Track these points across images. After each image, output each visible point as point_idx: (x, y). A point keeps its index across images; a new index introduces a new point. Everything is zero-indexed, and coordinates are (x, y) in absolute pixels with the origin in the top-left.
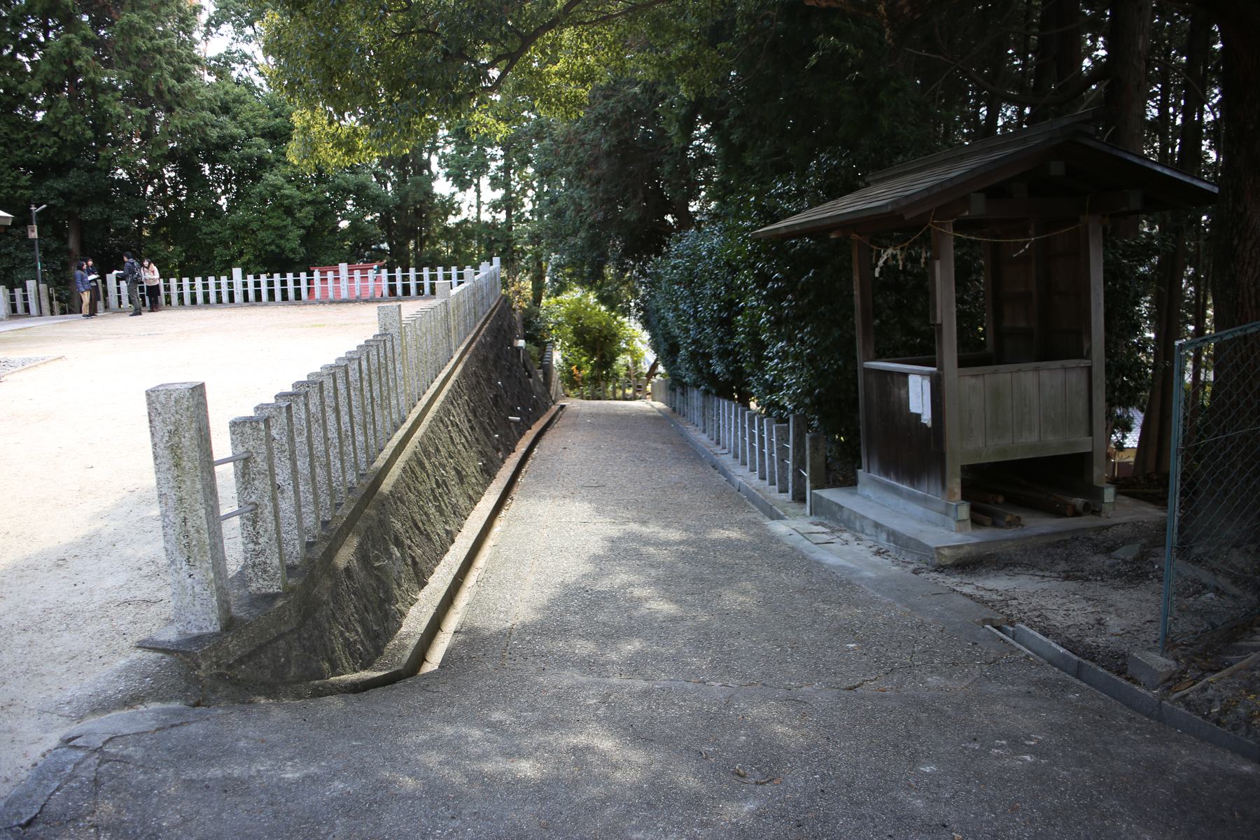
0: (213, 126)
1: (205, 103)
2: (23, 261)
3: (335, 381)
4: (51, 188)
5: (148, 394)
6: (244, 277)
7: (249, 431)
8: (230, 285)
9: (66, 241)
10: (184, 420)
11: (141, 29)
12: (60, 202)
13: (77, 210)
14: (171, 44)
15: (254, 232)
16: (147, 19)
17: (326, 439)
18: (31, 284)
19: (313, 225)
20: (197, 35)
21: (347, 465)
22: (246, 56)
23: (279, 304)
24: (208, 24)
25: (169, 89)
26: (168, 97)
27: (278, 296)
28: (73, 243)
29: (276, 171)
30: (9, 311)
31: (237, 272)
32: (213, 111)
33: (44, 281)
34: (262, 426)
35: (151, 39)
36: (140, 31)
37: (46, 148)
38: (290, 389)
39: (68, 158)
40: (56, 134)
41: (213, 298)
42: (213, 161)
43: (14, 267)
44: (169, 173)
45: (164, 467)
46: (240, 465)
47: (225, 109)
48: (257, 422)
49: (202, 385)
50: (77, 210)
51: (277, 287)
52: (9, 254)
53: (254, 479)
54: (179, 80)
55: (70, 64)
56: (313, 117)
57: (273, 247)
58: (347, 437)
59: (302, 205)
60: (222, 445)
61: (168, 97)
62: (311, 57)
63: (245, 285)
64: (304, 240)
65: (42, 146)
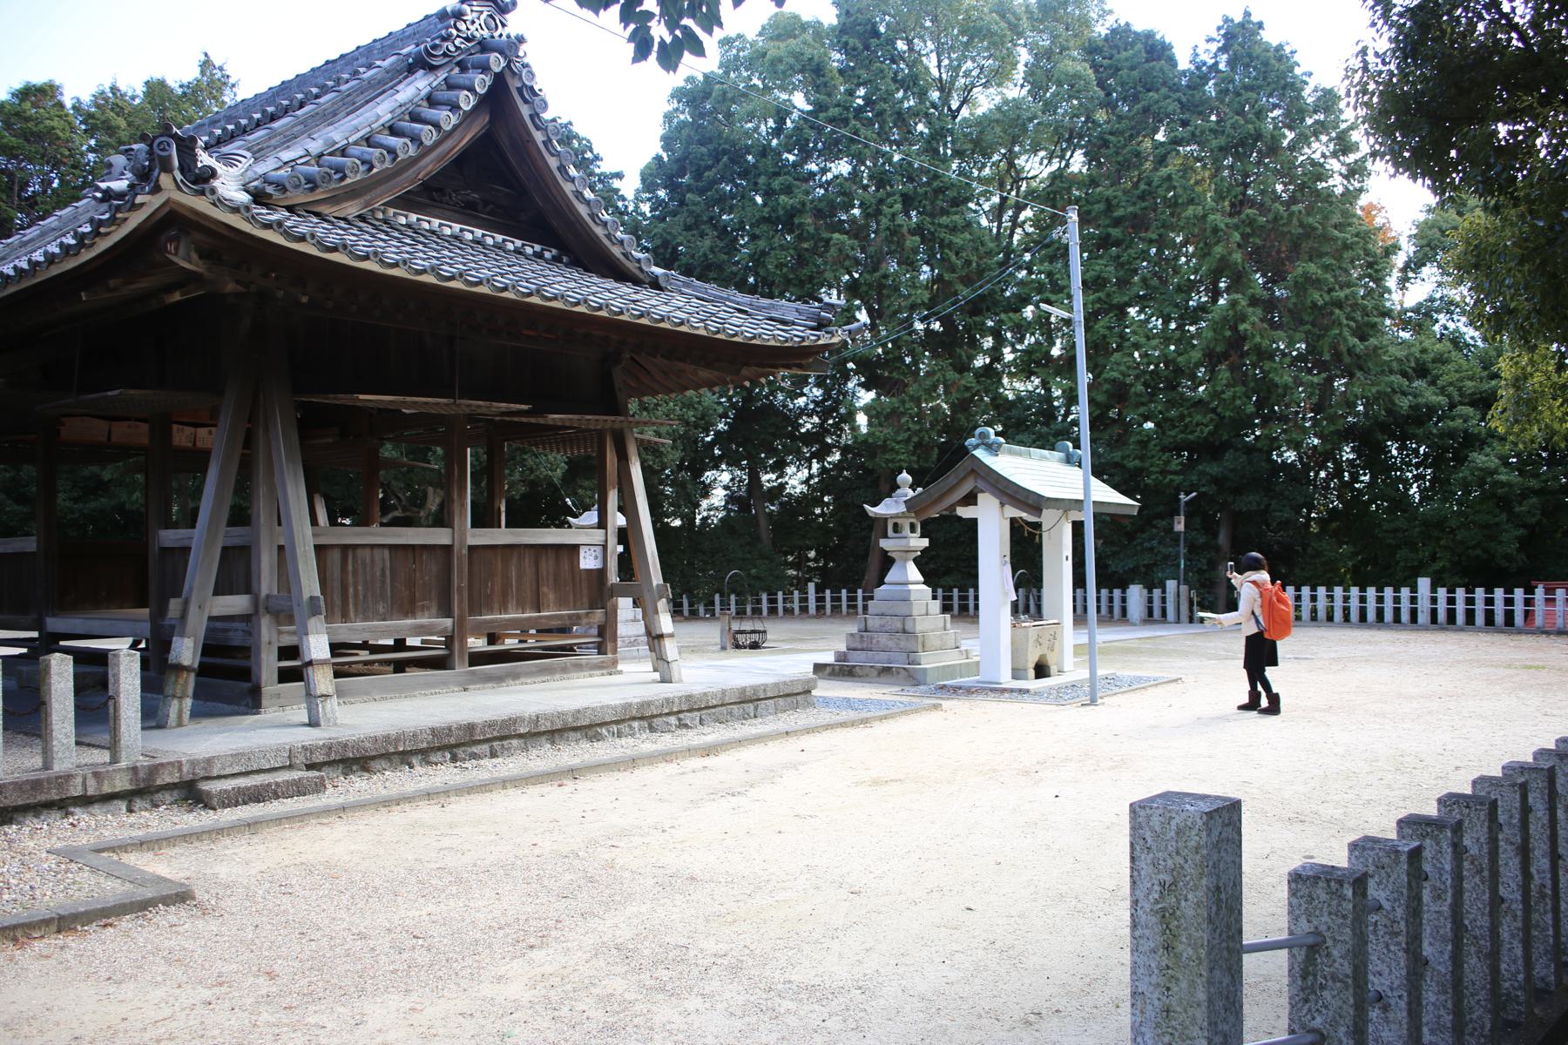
0: (1404, 394)
1: (1394, 364)
2: (1166, 557)
3: (1524, 797)
4: (1203, 473)
5: (1135, 809)
6: (1434, 590)
7: (1324, 897)
8: (1413, 600)
9: (1216, 535)
10: (1189, 868)
11: (1318, 281)
12: (1209, 489)
13: (1230, 499)
14: (1354, 294)
15: (1452, 531)
16: (1326, 268)
17: (1496, 901)
18: (1171, 585)
19: (1539, 523)
20: (1391, 282)
21: (1538, 948)
22: (1451, 303)
23: (1480, 630)
24: (1404, 270)
25: (1349, 350)
26: (1347, 360)
27: (1480, 619)
28: (1223, 539)
29: (1488, 450)
30: (1144, 614)
31: (1424, 584)
32: (1404, 374)
33: (1186, 582)
34: (1349, 892)
35: (1330, 291)
36: (1317, 283)
37: (1203, 426)
38: (1432, 810)
39: (1225, 437)
40: (1214, 410)
41: (1389, 616)
42: (1402, 441)
43: (1155, 564)
44: (1347, 454)
45: (1146, 946)
46: (1301, 955)
47: (1422, 371)
48: (1340, 883)
49: (1235, 806)
50: (1230, 499)
51: (1480, 607)
52: (1152, 549)
53: (1322, 987)
54: (1363, 339)
55: (1234, 329)
56: (1532, 362)
57: (1479, 552)
58: (1543, 896)
59: (1524, 496)
60: (1265, 910)
61: (1347, 360)
62: (1521, 262)
63: (1434, 600)
64: (1524, 543)
65: (1198, 424)
